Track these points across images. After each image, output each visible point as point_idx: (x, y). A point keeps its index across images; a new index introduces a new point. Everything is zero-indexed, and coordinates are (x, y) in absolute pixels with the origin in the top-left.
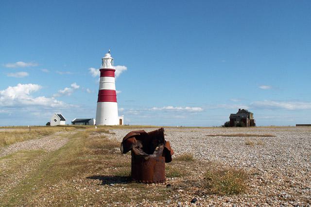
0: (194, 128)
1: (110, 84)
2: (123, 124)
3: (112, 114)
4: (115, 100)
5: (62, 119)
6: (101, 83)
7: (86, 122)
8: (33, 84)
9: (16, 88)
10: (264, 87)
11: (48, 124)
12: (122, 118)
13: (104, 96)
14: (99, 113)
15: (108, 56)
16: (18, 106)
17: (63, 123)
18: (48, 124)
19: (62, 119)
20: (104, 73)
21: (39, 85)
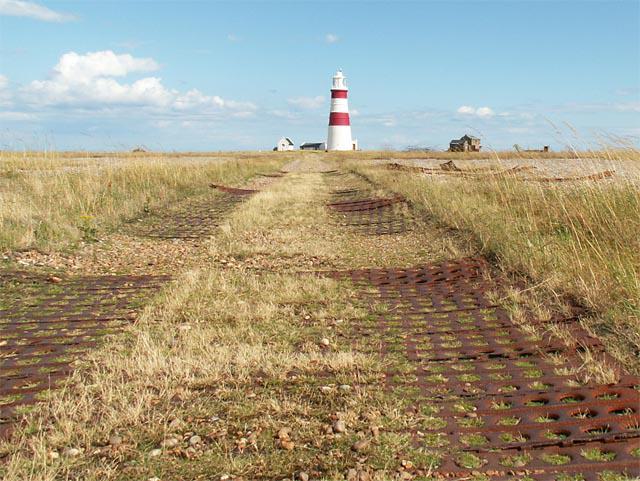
0: (198, 155)
1: (342, 105)
2: (356, 148)
3: (344, 139)
4: (348, 124)
5: (291, 144)
6: (333, 106)
7: (317, 146)
8: (117, 54)
9: (83, 58)
10: (331, 38)
11: (276, 149)
12: (356, 143)
13: (335, 119)
14: (331, 136)
15: (340, 75)
16: (81, 110)
17: (291, 148)
18: (276, 149)
19: (291, 144)
20: (335, 94)
21: (118, 52)
